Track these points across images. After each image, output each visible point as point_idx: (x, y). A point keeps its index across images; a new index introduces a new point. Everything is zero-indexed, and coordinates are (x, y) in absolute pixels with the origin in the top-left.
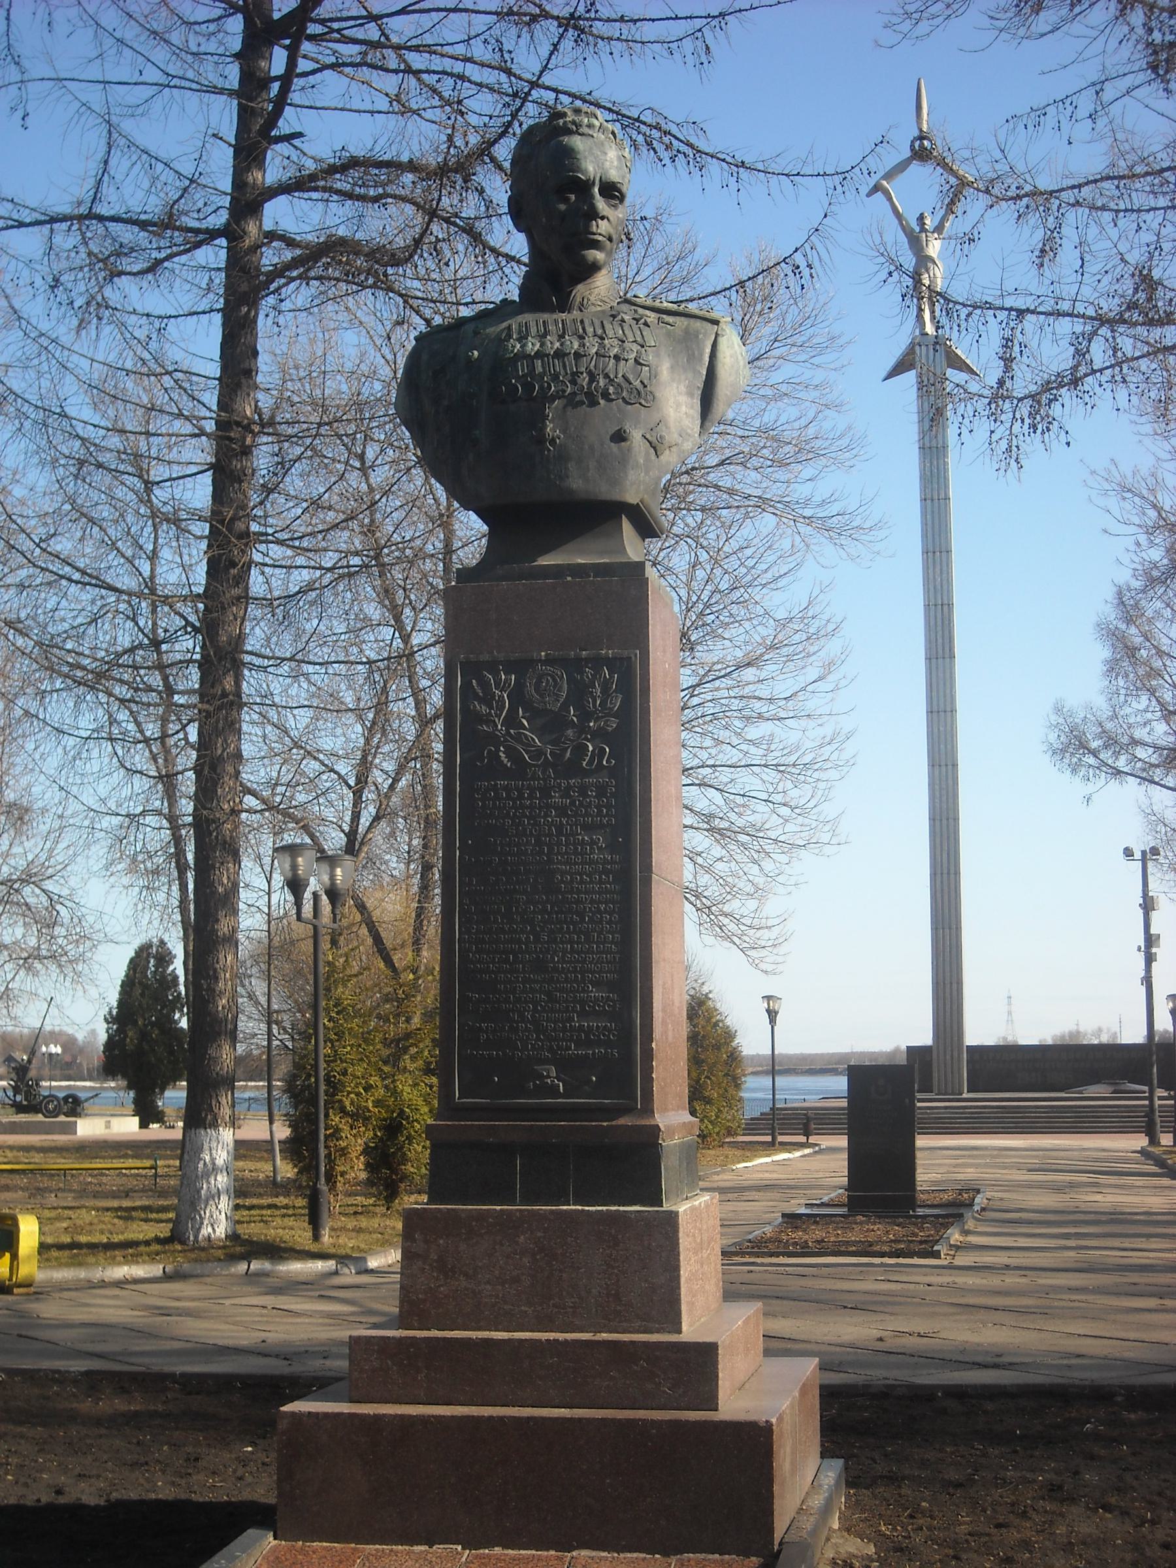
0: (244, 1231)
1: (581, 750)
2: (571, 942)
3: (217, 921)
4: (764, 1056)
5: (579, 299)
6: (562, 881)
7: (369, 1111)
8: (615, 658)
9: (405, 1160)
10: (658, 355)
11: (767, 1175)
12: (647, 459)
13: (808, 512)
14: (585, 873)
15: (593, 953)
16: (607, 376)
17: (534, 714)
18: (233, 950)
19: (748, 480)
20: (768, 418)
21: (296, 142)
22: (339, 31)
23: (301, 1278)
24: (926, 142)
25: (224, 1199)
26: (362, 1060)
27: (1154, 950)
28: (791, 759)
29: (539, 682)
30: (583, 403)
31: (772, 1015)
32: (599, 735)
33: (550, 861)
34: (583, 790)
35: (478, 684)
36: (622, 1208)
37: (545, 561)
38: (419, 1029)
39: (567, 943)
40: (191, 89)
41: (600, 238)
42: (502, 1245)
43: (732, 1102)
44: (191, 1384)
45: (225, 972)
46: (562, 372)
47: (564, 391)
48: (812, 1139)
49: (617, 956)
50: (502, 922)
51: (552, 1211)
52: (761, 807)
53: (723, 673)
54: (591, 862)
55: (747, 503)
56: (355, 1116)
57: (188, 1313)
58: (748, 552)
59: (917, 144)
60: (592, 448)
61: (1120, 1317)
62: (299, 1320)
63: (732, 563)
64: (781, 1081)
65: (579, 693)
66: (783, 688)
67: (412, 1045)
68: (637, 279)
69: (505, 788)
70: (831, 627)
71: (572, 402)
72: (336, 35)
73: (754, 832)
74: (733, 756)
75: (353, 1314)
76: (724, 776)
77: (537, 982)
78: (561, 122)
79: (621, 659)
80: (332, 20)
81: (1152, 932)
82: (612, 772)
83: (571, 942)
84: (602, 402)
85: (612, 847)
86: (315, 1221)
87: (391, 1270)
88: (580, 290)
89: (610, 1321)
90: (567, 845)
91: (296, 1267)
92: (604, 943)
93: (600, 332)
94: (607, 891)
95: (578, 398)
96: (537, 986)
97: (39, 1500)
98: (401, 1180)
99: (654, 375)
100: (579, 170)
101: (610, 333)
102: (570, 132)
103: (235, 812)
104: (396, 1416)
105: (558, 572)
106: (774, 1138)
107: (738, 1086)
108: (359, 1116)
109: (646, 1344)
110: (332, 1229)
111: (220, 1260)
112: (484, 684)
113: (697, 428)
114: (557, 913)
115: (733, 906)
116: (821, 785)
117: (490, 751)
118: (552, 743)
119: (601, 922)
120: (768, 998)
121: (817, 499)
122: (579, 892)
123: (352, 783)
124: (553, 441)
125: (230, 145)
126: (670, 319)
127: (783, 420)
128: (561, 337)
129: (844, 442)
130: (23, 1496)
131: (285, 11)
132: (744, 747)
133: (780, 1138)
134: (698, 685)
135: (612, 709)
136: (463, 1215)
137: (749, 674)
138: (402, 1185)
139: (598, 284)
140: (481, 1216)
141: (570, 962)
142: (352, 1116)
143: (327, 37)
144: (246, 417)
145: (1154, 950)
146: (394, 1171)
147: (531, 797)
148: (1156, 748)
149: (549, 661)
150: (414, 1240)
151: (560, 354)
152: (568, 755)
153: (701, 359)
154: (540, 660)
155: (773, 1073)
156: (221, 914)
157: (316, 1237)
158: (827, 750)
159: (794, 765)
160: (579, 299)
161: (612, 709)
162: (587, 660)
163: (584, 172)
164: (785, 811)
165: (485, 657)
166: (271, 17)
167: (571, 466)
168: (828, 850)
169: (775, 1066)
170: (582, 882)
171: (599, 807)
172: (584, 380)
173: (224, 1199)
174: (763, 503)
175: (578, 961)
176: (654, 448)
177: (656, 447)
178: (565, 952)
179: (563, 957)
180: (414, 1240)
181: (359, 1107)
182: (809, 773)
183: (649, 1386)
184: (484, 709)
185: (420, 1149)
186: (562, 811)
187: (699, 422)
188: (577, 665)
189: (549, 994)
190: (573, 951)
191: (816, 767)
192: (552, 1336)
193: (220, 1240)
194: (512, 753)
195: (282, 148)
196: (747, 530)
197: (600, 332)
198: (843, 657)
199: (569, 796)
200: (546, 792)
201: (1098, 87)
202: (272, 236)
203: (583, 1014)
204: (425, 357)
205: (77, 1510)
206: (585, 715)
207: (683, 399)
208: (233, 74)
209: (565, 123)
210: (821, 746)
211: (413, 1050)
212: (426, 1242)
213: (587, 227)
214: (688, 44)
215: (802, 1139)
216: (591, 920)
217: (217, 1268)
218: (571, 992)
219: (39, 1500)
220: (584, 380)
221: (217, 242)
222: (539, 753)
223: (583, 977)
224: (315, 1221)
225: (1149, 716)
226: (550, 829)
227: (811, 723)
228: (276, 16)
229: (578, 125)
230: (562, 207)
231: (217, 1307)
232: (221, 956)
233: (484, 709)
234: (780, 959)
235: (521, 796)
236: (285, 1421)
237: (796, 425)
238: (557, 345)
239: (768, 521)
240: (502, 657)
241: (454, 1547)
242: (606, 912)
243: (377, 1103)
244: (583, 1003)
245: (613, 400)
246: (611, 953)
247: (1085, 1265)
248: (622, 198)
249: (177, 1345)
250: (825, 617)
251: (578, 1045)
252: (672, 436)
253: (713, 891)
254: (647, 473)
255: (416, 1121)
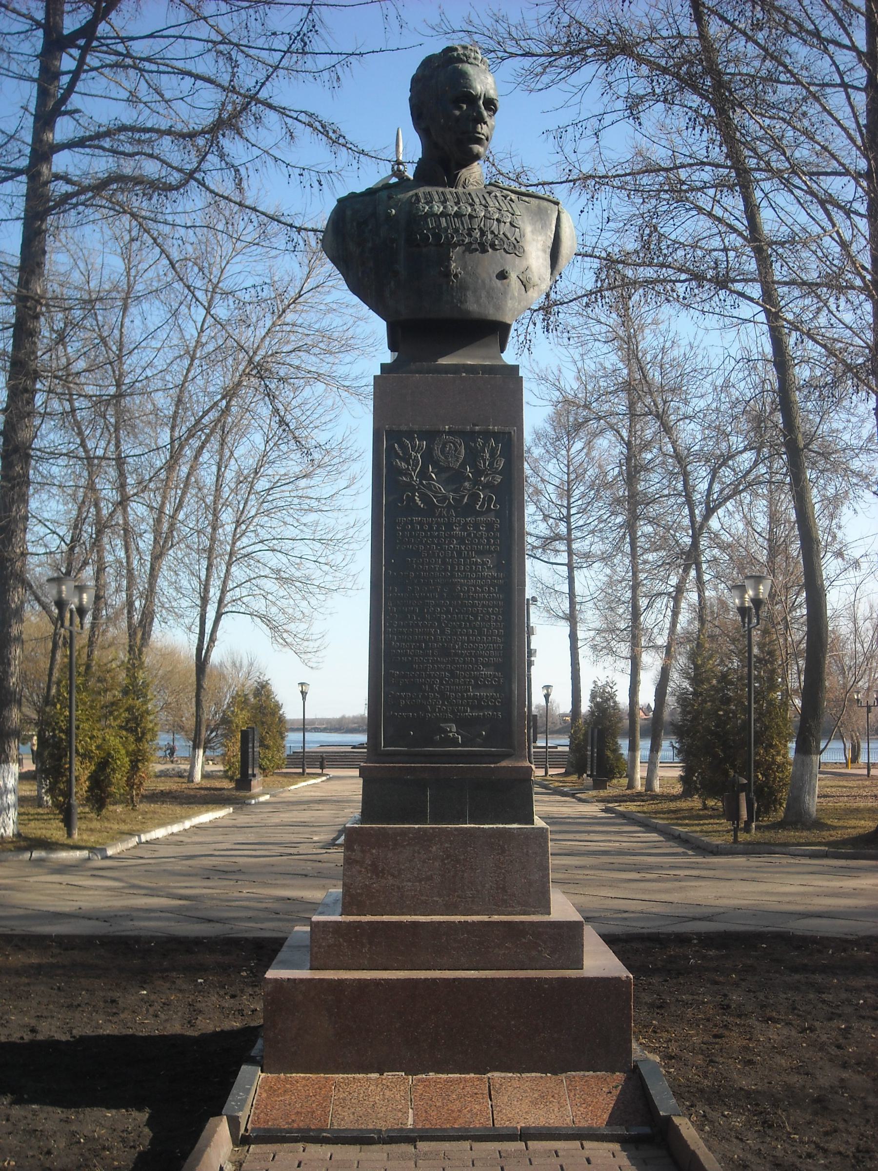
0: (24, 831)
1: (474, 497)
2: (467, 635)
3: (10, 626)
4: (362, 717)
5: (463, 179)
6: (461, 591)
7: (92, 752)
8: (499, 433)
9: (110, 784)
10: (523, 222)
11: (313, 794)
12: (520, 294)
13: (347, 383)
14: (478, 586)
15: (484, 643)
16: (492, 232)
17: (440, 470)
18: (20, 645)
19: (310, 362)
20: (324, 323)
21: (76, 116)
22: (107, 45)
23: (69, 863)
24: (401, 167)
25: (12, 810)
26: (88, 719)
27: (532, 659)
28: (329, 536)
29: (444, 446)
30: (477, 250)
31: (304, 694)
32: (488, 486)
33: (453, 576)
34: (476, 526)
35: (399, 447)
36: (507, 826)
37: (444, 361)
38: (120, 700)
39: (465, 635)
40: (7, 76)
41: (481, 136)
42: (419, 853)
43: (280, 748)
44: (66, 943)
45: (15, 660)
46: (461, 227)
47: (463, 241)
48: (325, 771)
49: (501, 645)
50: (417, 620)
51: (456, 829)
52: (312, 565)
53: (288, 481)
54: (482, 578)
55: (309, 376)
56: (84, 756)
57: (112, 896)
58: (307, 407)
59: (396, 167)
60: (483, 282)
61: (625, 885)
62: (85, 893)
63: (297, 412)
64: (309, 736)
65: (473, 456)
66: (327, 491)
67: (115, 710)
68: (244, 233)
69: (420, 523)
70: (357, 454)
71: (469, 249)
72: (105, 48)
73: (306, 581)
74: (290, 532)
75: (124, 888)
76: (287, 545)
77: (443, 663)
78: (455, 54)
79: (504, 433)
80: (103, 38)
81: (532, 647)
82: (498, 514)
83: (467, 635)
84: (490, 250)
85: (498, 567)
86: (68, 823)
87: (121, 856)
88: (464, 173)
89: (500, 907)
90: (465, 565)
91: (64, 855)
92: (492, 636)
93: (483, 202)
94: (493, 599)
95: (473, 247)
96: (443, 666)
97: (22, 1038)
98: (107, 797)
99: (523, 235)
100: (471, 87)
101: (491, 204)
102: (462, 61)
103: (24, 554)
104: (355, 980)
105: (456, 369)
106: (304, 771)
107: (283, 738)
108: (86, 756)
109: (532, 923)
110: (79, 829)
111: (11, 851)
112: (403, 447)
113: (549, 275)
114: (457, 614)
115: (292, 627)
116: (350, 553)
117: (408, 495)
118: (454, 491)
119: (490, 620)
120: (302, 684)
121: (353, 376)
122: (474, 599)
123: (68, 542)
124: (456, 276)
125: (32, 114)
126: (526, 199)
127: (334, 325)
128: (457, 203)
129: (371, 341)
130: (9, 1035)
131: (72, 29)
132: (302, 527)
133: (308, 771)
134: (272, 488)
135: (497, 469)
136: (390, 832)
137: (303, 483)
138: (108, 800)
139: (475, 170)
140: (403, 832)
141: (467, 649)
142: (81, 756)
143: (98, 49)
144: (36, 294)
145: (532, 659)
146: (103, 791)
147: (438, 530)
148: (538, 537)
149: (450, 433)
150: (353, 850)
151: (458, 215)
152: (465, 500)
153: (550, 228)
154: (444, 432)
155: (304, 730)
156: (13, 621)
157: (70, 835)
158: (351, 532)
159: (331, 540)
160: (463, 179)
161: (497, 469)
162: (479, 433)
163: (475, 89)
164: (326, 568)
165: (404, 428)
166: (62, 33)
167: (469, 294)
168: (350, 592)
169: (304, 726)
170: (476, 592)
171: (488, 538)
172: (477, 234)
173: (12, 810)
174: (318, 377)
175: (473, 649)
176: (525, 286)
177: (525, 285)
178: (463, 642)
179: (462, 646)
180: (353, 850)
181: (86, 750)
182: (341, 545)
183: (534, 953)
184: (404, 465)
185: (120, 777)
186: (461, 540)
187: (549, 271)
188: (472, 436)
189: (452, 673)
190: (469, 641)
191: (345, 541)
192: (462, 918)
193: (9, 837)
194: (424, 497)
195: (66, 118)
196: (307, 392)
197: (483, 202)
198: (362, 474)
199: (466, 530)
200: (449, 526)
201: (600, 117)
202: (57, 177)
203: (476, 687)
204: (349, 213)
205: (52, 1045)
206: (478, 473)
207: (540, 254)
208: (34, 69)
209: (458, 54)
210: (347, 529)
211: (116, 713)
212: (363, 851)
213: (475, 128)
214: (326, 74)
215: (319, 771)
216: (483, 620)
217: (10, 856)
218: (467, 670)
219: (22, 1038)
220: (477, 234)
221: (19, 178)
222: (445, 498)
223: (477, 661)
224: (68, 823)
225: (536, 517)
226: (452, 553)
227: (341, 514)
228: (66, 32)
229: (468, 57)
230: (457, 113)
231: (26, 884)
232: (13, 650)
233: (404, 465)
234: (321, 660)
235: (431, 528)
236: (270, 986)
237: (341, 329)
238: (456, 208)
239: (320, 387)
240: (416, 427)
241: (400, 1073)
242: (493, 614)
243: (98, 747)
244: (476, 678)
245: (497, 250)
246: (497, 643)
247: (567, 851)
248: (495, 111)
249: (21, 912)
250: (354, 448)
251: (473, 708)
252: (535, 279)
253: (281, 618)
254: (519, 303)
255: (119, 759)
